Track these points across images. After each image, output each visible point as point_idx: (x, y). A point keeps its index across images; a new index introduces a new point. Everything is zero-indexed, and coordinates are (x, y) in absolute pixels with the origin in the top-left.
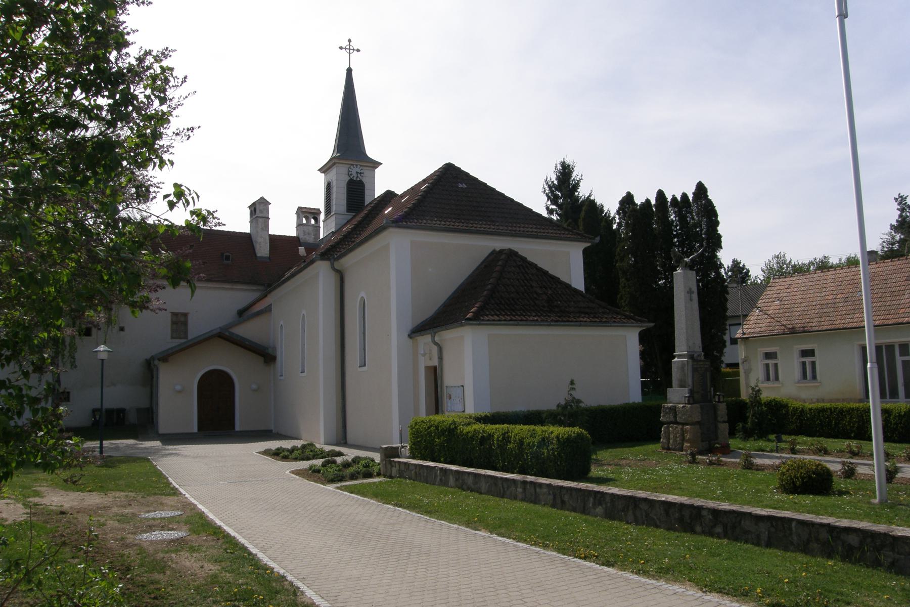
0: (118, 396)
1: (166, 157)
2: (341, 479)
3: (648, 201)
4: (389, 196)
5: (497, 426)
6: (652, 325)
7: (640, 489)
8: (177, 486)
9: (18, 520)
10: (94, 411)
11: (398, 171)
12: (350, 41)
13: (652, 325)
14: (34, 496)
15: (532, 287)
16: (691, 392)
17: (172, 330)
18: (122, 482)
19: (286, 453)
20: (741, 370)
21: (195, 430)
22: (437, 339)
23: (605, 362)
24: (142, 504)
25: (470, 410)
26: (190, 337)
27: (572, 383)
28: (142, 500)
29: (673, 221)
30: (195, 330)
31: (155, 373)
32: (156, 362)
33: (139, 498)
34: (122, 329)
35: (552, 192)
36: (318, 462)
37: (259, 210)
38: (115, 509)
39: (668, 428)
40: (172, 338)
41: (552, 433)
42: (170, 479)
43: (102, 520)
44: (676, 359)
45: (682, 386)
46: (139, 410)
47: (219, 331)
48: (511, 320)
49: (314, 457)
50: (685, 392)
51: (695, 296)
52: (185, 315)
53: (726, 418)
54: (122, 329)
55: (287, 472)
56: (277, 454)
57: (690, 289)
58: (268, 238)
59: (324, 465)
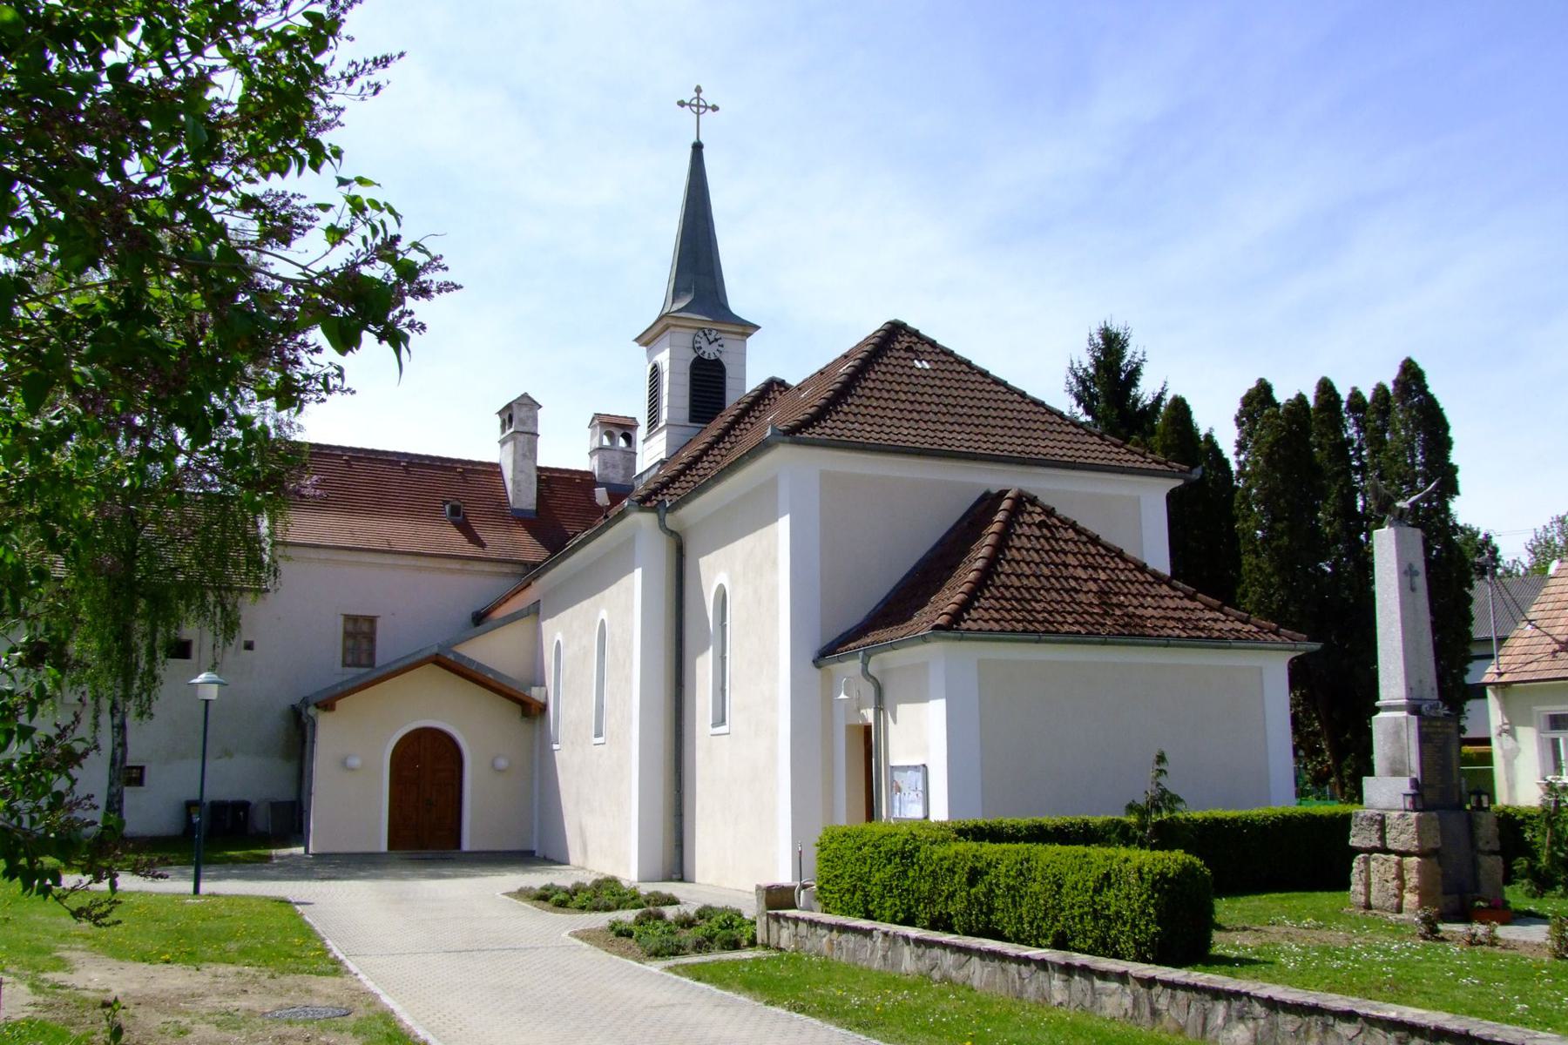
0: (240, 777)
1: (325, 138)
2: (677, 950)
3: (1301, 398)
4: (774, 387)
5: (1005, 846)
6: (1316, 646)
7: (1330, 990)
8: (341, 957)
9: (16, 1017)
10: (190, 805)
11: (794, 334)
12: (698, 90)
13: (1316, 646)
14: (54, 969)
15: (1066, 566)
16: (1415, 783)
17: (346, 650)
18: (233, 946)
19: (562, 897)
20: (1496, 748)
21: (384, 847)
22: (872, 669)
23: (1223, 720)
24: (270, 991)
25: (940, 812)
26: (379, 662)
27: (1161, 758)
28: (268, 983)
29: (1350, 441)
30: (387, 649)
31: (309, 735)
32: (312, 711)
33: (264, 978)
34: (249, 646)
35: (1086, 389)
36: (628, 916)
37: (519, 417)
38: (213, 1001)
39: (1366, 861)
40: (345, 664)
41: (1127, 860)
42: (329, 942)
43: (185, 1021)
44: (1381, 715)
45: (1396, 772)
46: (275, 806)
47: (435, 650)
48: (1025, 631)
49: (618, 906)
50: (1404, 785)
51: (1421, 581)
52: (372, 620)
53: (1496, 846)
54: (249, 646)
55: (565, 935)
56: (544, 897)
57: (1411, 566)
58: (534, 474)
59: (639, 922)
